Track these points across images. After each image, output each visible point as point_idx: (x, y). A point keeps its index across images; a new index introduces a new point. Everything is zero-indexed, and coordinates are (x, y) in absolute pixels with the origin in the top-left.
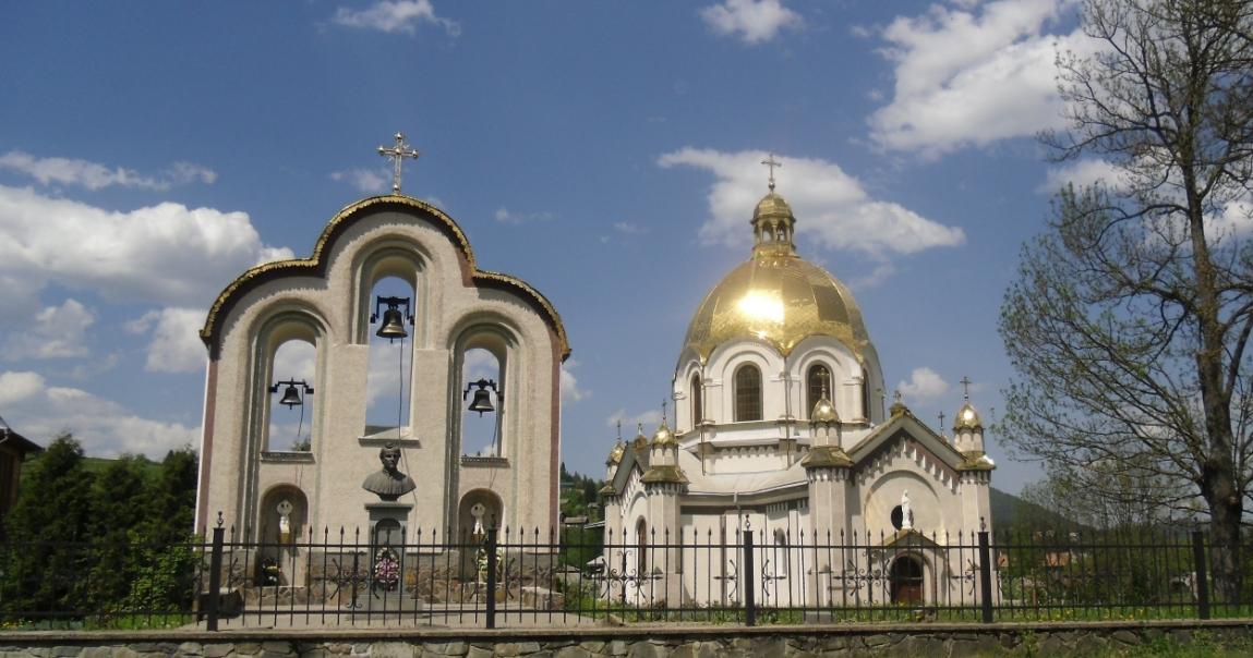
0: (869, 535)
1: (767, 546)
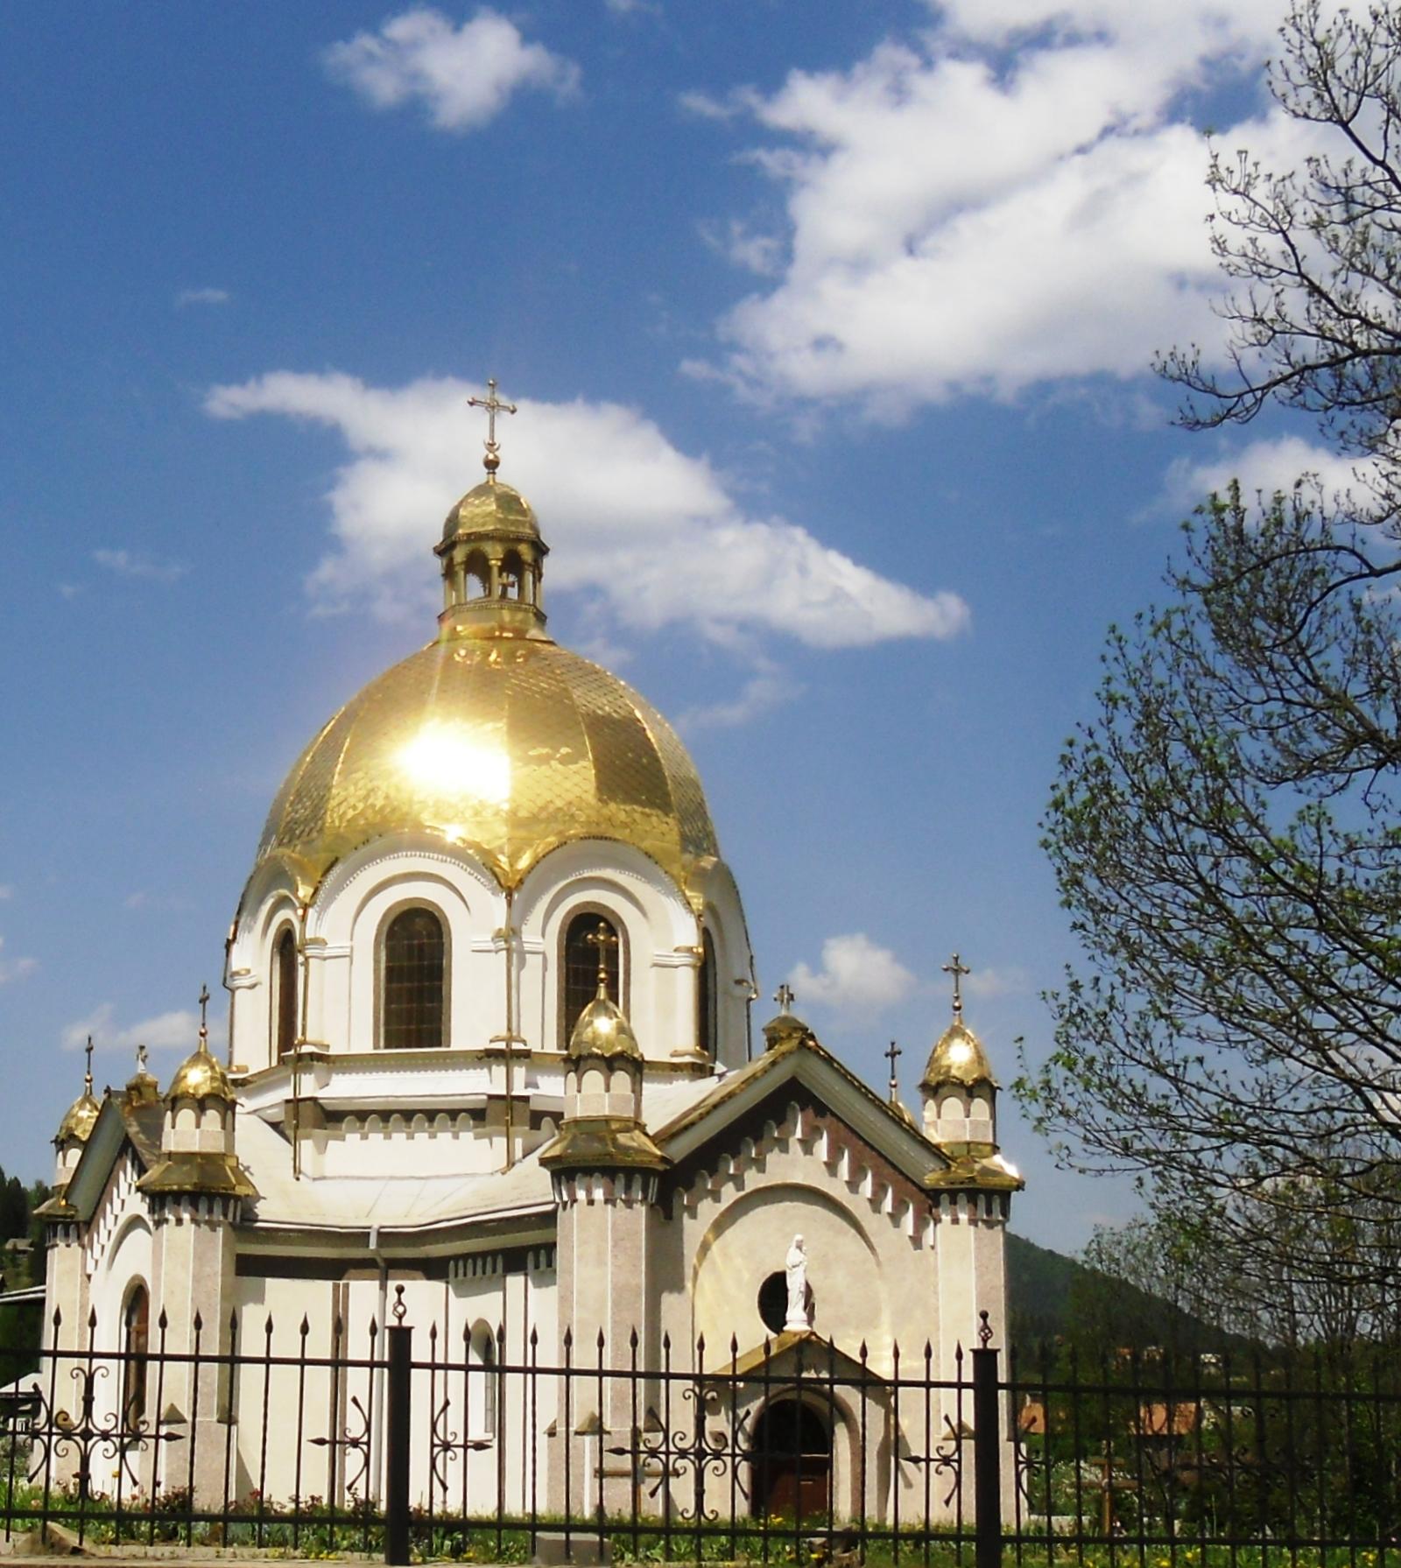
0: (534, 1340)
1: (447, 1367)
